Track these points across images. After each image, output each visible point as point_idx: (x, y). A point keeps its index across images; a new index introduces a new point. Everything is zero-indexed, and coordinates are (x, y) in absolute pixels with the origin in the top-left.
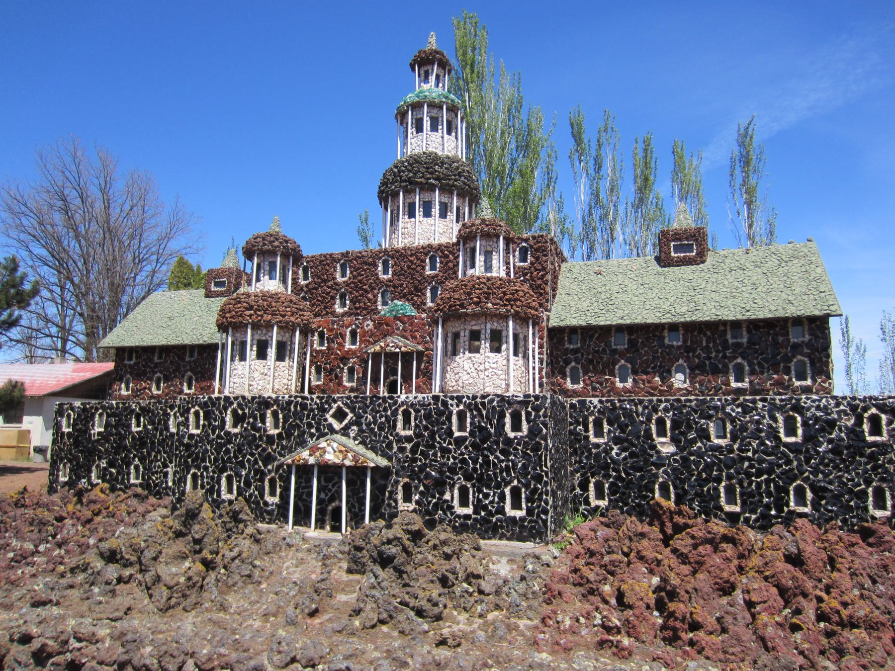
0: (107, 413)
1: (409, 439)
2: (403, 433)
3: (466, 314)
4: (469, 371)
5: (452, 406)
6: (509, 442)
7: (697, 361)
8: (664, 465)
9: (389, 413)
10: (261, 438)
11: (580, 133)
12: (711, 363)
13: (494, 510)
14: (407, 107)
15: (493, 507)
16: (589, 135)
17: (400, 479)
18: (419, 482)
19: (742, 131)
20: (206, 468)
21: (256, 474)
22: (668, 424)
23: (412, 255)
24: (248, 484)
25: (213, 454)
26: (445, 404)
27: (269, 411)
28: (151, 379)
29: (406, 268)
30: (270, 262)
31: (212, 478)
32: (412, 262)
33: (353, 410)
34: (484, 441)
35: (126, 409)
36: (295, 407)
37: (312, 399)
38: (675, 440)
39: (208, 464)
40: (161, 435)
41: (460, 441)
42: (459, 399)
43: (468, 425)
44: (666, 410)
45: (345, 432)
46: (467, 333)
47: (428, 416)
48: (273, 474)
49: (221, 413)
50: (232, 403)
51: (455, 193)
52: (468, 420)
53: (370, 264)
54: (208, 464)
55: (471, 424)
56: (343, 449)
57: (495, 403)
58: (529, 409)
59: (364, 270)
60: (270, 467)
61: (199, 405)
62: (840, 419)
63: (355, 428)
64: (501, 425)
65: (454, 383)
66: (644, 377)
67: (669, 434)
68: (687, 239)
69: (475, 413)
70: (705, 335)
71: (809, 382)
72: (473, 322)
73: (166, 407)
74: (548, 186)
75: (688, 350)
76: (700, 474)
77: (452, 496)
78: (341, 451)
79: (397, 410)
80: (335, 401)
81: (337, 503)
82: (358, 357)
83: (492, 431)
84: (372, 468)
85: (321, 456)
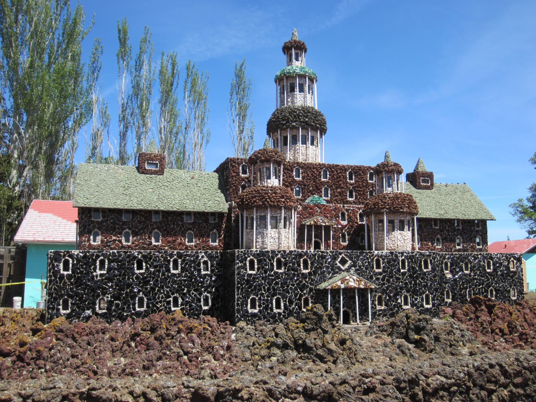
0: (109, 259)
1: (380, 274)
2: (377, 271)
3: (403, 212)
6: (425, 274)
8: (448, 283)
9: (370, 260)
10: (298, 275)
14: (296, 75)
16: (133, 42)
19: (238, 67)
21: (296, 296)
23: (314, 168)
24: (291, 302)
25: (266, 286)
27: (302, 260)
28: (120, 233)
29: (310, 175)
30: (266, 168)
32: (314, 172)
33: (351, 259)
34: (414, 273)
35: (129, 256)
37: (327, 253)
38: (451, 272)
40: (163, 274)
41: (404, 274)
42: (402, 253)
44: (448, 258)
45: (348, 270)
47: (389, 262)
50: (277, 255)
51: (310, 129)
52: (407, 264)
55: (408, 266)
60: (305, 292)
61: (253, 256)
62: (503, 262)
63: (353, 268)
64: (420, 266)
65: (392, 246)
66: (425, 243)
68: (427, 177)
71: (481, 247)
72: (401, 216)
73: (166, 255)
74: (93, 73)
75: (441, 231)
76: (460, 286)
78: (357, 281)
79: (373, 259)
80: (340, 254)
83: (417, 269)
84: (343, 289)
85: (347, 283)
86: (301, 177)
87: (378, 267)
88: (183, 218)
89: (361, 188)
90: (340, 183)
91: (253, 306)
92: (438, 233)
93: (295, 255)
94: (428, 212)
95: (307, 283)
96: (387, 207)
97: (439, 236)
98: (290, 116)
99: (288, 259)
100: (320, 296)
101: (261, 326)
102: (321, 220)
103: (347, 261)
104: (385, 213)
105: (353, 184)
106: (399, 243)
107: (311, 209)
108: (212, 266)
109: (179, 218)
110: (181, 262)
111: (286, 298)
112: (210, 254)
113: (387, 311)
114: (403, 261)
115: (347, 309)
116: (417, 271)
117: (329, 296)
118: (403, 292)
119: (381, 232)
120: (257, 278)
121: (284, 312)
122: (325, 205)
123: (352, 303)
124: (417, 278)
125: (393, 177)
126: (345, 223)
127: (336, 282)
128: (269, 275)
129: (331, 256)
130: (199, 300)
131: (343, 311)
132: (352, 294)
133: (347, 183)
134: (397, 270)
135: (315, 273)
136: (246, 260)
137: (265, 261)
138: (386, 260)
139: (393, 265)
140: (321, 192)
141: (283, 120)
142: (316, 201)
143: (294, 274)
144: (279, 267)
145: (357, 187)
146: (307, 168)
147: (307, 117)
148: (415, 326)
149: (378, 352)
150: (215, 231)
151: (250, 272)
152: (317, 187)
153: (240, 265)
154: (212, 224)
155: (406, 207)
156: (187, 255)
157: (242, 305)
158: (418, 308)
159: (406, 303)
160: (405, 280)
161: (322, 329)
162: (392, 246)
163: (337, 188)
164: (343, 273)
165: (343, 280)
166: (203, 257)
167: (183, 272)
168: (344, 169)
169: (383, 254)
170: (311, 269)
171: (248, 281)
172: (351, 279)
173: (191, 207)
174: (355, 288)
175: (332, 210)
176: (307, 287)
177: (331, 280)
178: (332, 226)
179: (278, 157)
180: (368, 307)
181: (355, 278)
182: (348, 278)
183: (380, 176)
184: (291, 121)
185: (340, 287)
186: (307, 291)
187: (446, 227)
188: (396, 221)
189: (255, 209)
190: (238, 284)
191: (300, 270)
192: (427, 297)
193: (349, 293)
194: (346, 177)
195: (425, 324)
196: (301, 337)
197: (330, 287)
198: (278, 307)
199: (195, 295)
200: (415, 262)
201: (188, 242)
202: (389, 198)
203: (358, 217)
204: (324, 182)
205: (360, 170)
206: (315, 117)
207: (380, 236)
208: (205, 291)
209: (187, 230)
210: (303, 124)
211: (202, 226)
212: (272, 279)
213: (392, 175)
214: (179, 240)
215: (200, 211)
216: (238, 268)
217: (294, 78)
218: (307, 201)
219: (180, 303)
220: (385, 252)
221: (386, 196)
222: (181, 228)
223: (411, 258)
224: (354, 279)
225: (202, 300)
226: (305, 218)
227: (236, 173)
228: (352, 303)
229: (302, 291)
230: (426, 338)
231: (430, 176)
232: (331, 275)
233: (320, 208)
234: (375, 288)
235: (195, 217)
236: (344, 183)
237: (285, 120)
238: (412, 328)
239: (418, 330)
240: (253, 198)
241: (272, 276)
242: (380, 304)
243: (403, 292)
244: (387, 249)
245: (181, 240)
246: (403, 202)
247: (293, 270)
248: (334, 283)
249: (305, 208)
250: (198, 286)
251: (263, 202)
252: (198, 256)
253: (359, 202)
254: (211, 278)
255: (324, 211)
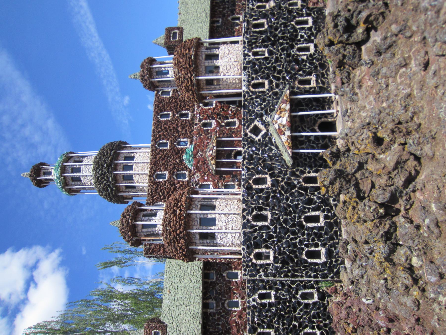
1: (271, 82)
2: (267, 87)
4: (229, 58)
5: (249, 59)
7: (229, 12)
8: (280, 4)
9: (254, 96)
10: (274, 192)
11: (110, 263)
12: (231, 7)
13: (310, 32)
14: (62, 176)
15: (308, 33)
17: (296, 86)
18: (297, 74)
20: (301, 242)
21: (302, 195)
22: (259, 4)
23: (156, 158)
24: (310, 201)
25: (289, 236)
26: (249, 62)
29: (163, 162)
31: (309, 235)
32: (160, 158)
33: (252, 121)
34: (270, 40)
36: (250, 164)
37: (245, 152)
39: (298, 240)
41: (270, 53)
42: (245, 55)
43: (261, 49)
46: (207, 61)
47: (256, 72)
48: (301, 180)
49: (255, 231)
50: (248, 220)
51: (116, 162)
53: (158, 186)
54: (298, 240)
55: (260, 47)
56: (279, 111)
57: (248, 36)
58: (252, 19)
59: (161, 191)
60: (296, 182)
61: (250, 254)
63: (264, 118)
64: (261, 33)
67: (264, 4)
69: (254, 46)
70: (217, 9)
72: (201, 58)
75: (224, 16)
77: (304, 56)
78: (281, 112)
79: (252, 92)
80: (246, 135)
81: (318, 130)
82: (218, 182)
83: (264, 36)
84: (292, 132)
86: (165, 172)
87: (262, 85)
88: (211, 313)
89: (178, 104)
90: (171, 128)
91: (317, 255)
92: (226, 19)
93: (248, 195)
94: (204, 31)
95: (283, 179)
96: (189, 75)
97: (229, 19)
98: (102, 183)
99: (253, 206)
100: (301, 162)
101: (347, 252)
102: (209, 151)
103: (255, 126)
104: (197, 78)
105: (173, 113)
106: (233, 60)
107: (198, 163)
108: (265, 288)
109: (211, 318)
110: (260, 328)
111: (305, 208)
112: (250, 290)
113: (318, 73)
114: (255, 54)
115: (317, 125)
116: (267, 36)
117: (302, 151)
118: (293, 53)
119: (221, 83)
120: (280, 249)
121: (323, 211)
122: (195, 146)
123: (308, 119)
124: (275, 36)
125: (157, 70)
126: (214, 123)
127: (282, 142)
128: (275, 232)
129: (249, 147)
130: (307, 305)
131: (322, 131)
132: (297, 119)
133: (172, 120)
134: (266, 61)
135: (271, 168)
136: (256, 265)
137: (256, 238)
138: (254, 76)
139: (260, 66)
140: (182, 149)
141: (108, 190)
142: (190, 156)
143: (274, 197)
144: (264, 218)
145: (176, 109)
146: (155, 165)
147: (103, 166)
148: (344, 33)
149: (387, 86)
150: (225, 274)
151: (272, 258)
152: (177, 154)
153: (262, 273)
154: (217, 278)
155: (189, 51)
156: (253, 321)
157: (316, 271)
158: (312, 34)
159: (307, 49)
160: (279, 51)
161: (356, 172)
162: (236, 69)
163: (178, 131)
164: (270, 132)
165: (280, 132)
166: (254, 300)
167: (273, 326)
168: (157, 123)
169: (246, 80)
170: (266, 174)
171: (284, 263)
172: (279, 122)
173: (197, 307)
174: (290, 117)
175: (200, 138)
176: (289, 179)
177: (281, 147)
178: (217, 137)
179: (129, 215)
180: (314, 98)
181: (276, 116)
182: (276, 126)
183: (158, 84)
184: (108, 182)
185: (288, 136)
186: (295, 180)
187: (220, 11)
188: (207, 64)
189: (190, 247)
190: (288, 276)
191: (267, 189)
192: (298, 23)
193: (296, 122)
194: (165, 121)
195: (340, 19)
196: (374, 210)
197: (290, 151)
198: (316, 219)
199: (301, 310)
200: (256, 39)
201: (237, 307)
202: (179, 73)
203: (207, 108)
204: (170, 146)
205: (158, 106)
206: (104, 156)
207: (225, 83)
208: (295, 298)
209: (225, 308)
210: (110, 170)
211: (220, 290)
212: (280, 228)
213: (155, 70)
214: (236, 318)
215: (201, 296)
216: (267, 276)
217: (65, 178)
218: (190, 167)
219: (311, 331)
220: (244, 77)
221: (178, 76)
222: (222, 316)
223: (250, 44)
224: (279, 118)
225: (306, 301)
226: (209, 170)
227: (160, 247)
228: (311, 120)
229: (295, 186)
230: (364, 15)
231: (169, 30)
232: (273, 147)
233: (198, 152)
234: (289, 89)
235: (210, 298)
236: (172, 123)
237: (107, 188)
238: (348, 37)
239: (350, 28)
240: (176, 249)
241: (276, 228)
242: (308, 82)
243: (293, 53)
244: (241, 75)
245: (235, 316)
246: (183, 56)
247: (267, 198)
248: (284, 145)
249: (197, 168)
250: (289, 307)
251: (180, 238)
252: (253, 306)
253: (192, 106)
254: (280, 290)
255: (200, 147)
